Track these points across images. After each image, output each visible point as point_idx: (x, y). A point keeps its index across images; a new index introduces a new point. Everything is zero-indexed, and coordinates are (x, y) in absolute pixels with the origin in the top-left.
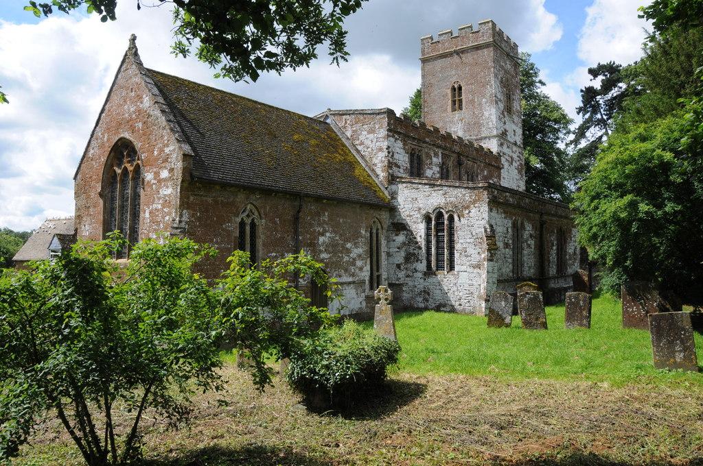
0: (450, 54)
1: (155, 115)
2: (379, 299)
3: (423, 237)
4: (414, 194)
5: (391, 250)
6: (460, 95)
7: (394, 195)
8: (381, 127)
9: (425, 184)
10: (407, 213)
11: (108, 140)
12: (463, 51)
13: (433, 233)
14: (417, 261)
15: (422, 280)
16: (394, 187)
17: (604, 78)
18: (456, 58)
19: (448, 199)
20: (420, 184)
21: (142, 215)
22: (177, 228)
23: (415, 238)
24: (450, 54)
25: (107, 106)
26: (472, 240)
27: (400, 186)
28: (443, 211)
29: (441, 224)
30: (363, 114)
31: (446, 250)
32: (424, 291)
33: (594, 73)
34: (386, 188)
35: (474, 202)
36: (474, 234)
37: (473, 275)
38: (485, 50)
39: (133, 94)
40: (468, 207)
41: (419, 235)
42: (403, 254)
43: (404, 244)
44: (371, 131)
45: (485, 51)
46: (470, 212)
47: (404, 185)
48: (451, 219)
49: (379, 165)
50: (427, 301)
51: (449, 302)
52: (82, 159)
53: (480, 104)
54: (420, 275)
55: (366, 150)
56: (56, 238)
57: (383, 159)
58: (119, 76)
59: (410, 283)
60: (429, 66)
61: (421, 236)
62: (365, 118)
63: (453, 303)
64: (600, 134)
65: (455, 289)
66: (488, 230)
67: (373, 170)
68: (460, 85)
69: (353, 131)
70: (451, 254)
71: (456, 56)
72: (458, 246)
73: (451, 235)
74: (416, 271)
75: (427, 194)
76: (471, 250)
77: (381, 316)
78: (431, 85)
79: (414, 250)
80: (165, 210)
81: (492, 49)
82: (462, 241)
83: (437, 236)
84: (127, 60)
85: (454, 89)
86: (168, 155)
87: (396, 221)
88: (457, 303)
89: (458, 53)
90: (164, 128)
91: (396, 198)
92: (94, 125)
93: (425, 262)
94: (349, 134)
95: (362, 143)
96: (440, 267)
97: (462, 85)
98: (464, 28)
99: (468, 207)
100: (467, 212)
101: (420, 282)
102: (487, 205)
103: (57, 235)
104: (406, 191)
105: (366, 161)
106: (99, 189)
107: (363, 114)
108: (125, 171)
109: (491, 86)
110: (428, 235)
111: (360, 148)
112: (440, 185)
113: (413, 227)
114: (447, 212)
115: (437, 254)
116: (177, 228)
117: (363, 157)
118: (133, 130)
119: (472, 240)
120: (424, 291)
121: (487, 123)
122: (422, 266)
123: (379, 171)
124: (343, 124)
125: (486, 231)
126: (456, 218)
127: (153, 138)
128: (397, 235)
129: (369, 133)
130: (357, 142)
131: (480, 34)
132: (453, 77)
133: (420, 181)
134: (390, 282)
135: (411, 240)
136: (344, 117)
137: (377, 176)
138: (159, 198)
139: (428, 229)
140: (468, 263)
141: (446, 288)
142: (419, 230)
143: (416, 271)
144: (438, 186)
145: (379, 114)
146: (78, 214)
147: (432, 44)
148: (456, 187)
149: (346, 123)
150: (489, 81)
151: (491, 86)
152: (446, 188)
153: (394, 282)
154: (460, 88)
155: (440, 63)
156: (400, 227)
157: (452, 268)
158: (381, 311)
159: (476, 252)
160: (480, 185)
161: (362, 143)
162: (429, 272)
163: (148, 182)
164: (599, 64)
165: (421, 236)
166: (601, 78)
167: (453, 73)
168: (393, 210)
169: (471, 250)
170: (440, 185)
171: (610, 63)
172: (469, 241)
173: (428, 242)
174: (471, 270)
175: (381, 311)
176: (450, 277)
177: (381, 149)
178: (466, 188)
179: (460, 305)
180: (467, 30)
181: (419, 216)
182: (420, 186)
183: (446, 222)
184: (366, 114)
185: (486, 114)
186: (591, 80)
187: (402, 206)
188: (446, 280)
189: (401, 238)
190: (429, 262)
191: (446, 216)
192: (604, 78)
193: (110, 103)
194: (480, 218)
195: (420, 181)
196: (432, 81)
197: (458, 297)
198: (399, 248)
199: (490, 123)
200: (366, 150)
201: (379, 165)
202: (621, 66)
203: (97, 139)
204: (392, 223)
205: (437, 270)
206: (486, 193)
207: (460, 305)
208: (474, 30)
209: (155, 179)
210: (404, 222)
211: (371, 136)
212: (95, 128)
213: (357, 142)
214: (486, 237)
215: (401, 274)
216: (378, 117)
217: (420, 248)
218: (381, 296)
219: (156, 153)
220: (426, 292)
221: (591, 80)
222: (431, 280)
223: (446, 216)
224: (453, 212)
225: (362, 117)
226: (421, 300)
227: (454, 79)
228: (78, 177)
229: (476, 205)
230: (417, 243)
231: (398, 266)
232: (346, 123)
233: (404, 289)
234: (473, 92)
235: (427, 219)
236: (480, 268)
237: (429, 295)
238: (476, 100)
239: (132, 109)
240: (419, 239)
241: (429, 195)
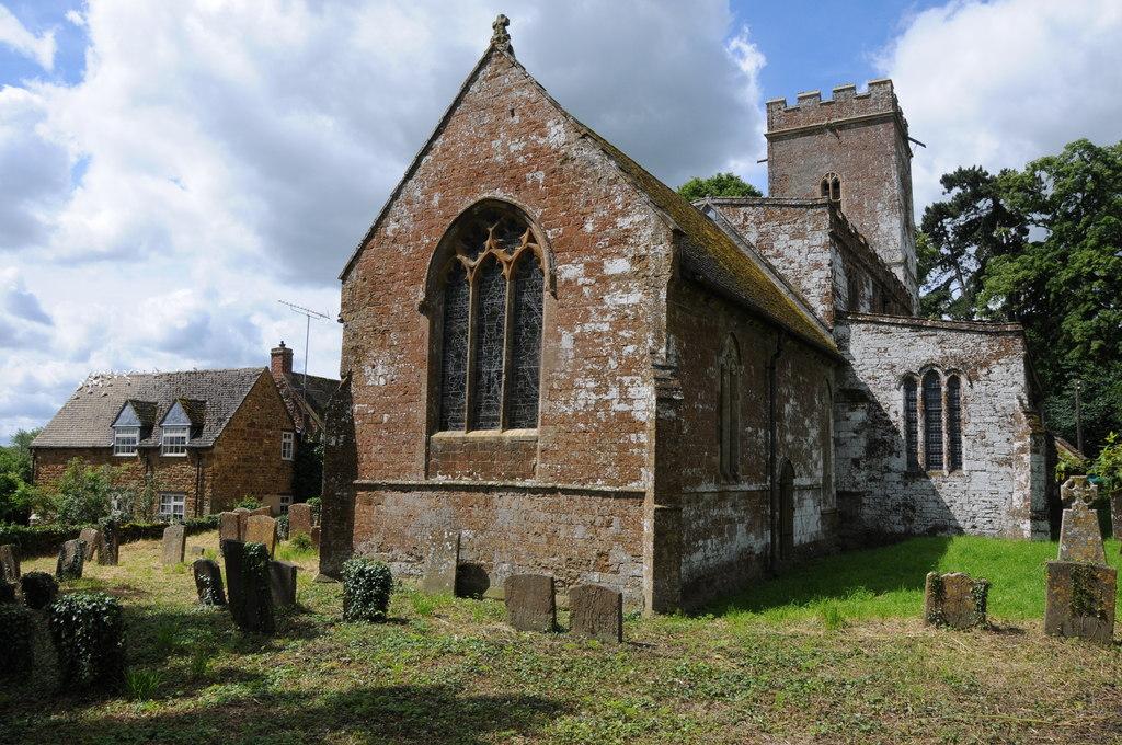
0: (820, 130)
1: (584, 159)
2: (1071, 499)
3: (901, 412)
4: (881, 341)
5: (842, 435)
6: (837, 194)
7: (843, 341)
8: (818, 228)
9: (903, 325)
10: (869, 373)
11: (443, 204)
12: (842, 126)
13: (919, 405)
14: (891, 454)
15: (901, 486)
16: (841, 330)
17: (961, 191)
18: (829, 137)
19: (948, 351)
20: (893, 324)
21: (546, 345)
22: (663, 368)
23: (886, 415)
24: (820, 130)
25: (439, 143)
26: (995, 419)
27: (854, 328)
28: (939, 370)
29: (935, 393)
30: (781, 206)
31: (945, 436)
32: (905, 505)
33: (949, 182)
34: (830, 331)
35: (998, 356)
36: (998, 408)
37: (998, 477)
38: (880, 126)
39: (517, 119)
40: (986, 364)
41: (893, 409)
42: (863, 441)
43: (864, 424)
44: (799, 235)
45: (881, 128)
46: (990, 372)
47: (863, 326)
48: (954, 383)
49: (815, 292)
50: (911, 521)
51: (952, 523)
52: (370, 236)
53: (873, 211)
54: (896, 477)
55: (787, 265)
56: (129, 408)
57: (823, 282)
58: (474, 88)
59: (878, 492)
60: (781, 147)
61: (896, 412)
62: (785, 213)
63: (961, 524)
64: (944, 279)
65: (964, 499)
66: (1026, 402)
67: (804, 302)
68: (836, 180)
69: (762, 234)
70: (955, 442)
71: (829, 133)
72: (968, 429)
73: (954, 410)
74: (889, 470)
75: (907, 341)
76: (993, 435)
77: (1076, 530)
78: (785, 177)
79: (883, 434)
80: (621, 333)
81: (892, 124)
82: (977, 421)
83: (926, 412)
84: (494, 60)
85: (825, 186)
86: (626, 230)
87: (847, 386)
88: (968, 524)
89: (832, 128)
90: (613, 182)
91: (846, 348)
92: (402, 176)
93: (904, 455)
94: (752, 237)
95: (779, 255)
96: (933, 462)
97: (840, 179)
98: (843, 90)
99: (986, 364)
100: (985, 371)
101: (898, 492)
102: (1022, 360)
103: (134, 402)
104: (866, 337)
105: (787, 285)
106: (421, 296)
107: (781, 206)
108: (491, 264)
109: (891, 183)
110: (909, 410)
111: (774, 262)
112: (930, 328)
113: (881, 397)
114: (946, 373)
115: (927, 442)
116: (663, 368)
117: (781, 278)
118: (517, 183)
119: (995, 419)
120: (905, 505)
121: (886, 242)
122: (899, 463)
123: (814, 301)
124: (740, 221)
125: (1022, 403)
126: (964, 382)
127: (579, 201)
128: (852, 410)
129: (793, 237)
130: (769, 253)
131: (872, 100)
132: (826, 167)
133: (893, 320)
134: (840, 489)
135: (878, 416)
136: (742, 209)
137: (811, 310)
138: (604, 313)
139: (910, 400)
140: (988, 457)
141: (946, 499)
142: (894, 402)
143: (889, 470)
144: (926, 328)
145: (812, 206)
146: (354, 344)
147: (785, 111)
148: (964, 331)
149: (746, 219)
150: (888, 176)
151: (891, 183)
152: (943, 333)
153: (847, 489)
154: (836, 185)
155: (799, 144)
156: (859, 396)
157: (955, 464)
158: (1076, 521)
159: (1004, 438)
160: (1009, 328)
161: (779, 255)
162: (914, 473)
163: (568, 282)
164: (960, 169)
165: (896, 412)
166: (957, 190)
167: (825, 159)
168: (841, 364)
169: (993, 435)
170: (930, 328)
171: (974, 168)
172: (989, 419)
173: (910, 422)
174: (996, 467)
175: (1076, 521)
176: (955, 480)
177: (818, 266)
178: (981, 333)
179: (974, 527)
180: (848, 93)
181: (891, 378)
182: (893, 328)
183: (944, 389)
184: (787, 206)
185: (884, 227)
186: (944, 193)
187: (858, 362)
188: (948, 486)
189: (859, 415)
190: (912, 453)
191: (944, 379)
192: (961, 191)
193: (447, 136)
194: (1010, 383)
195: (893, 320)
196: (787, 171)
197: (971, 514)
198: (855, 432)
199: (891, 243)
200: (787, 265)
201: (815, 292)
202: (987, 174)
203: (409, 203)
204: (841, 390)
205: (928, 468)
206: (1019, 341)
207: (974, 527)
208: (790, 107)
209: (587, 275)
210: (864, 388)
211: (798, 243)
212: (405, 181)
213: (769, 253)
214: (1025, 412)
215: (861, 476)
216: (811, 212)
217: (896, 432)
218: (1076, 494)
219: (589, 227)
220: (909, 507)
221: (944, 193)
222: (919, 485)
223: (944, 379)
224: (959, 372)
225: (778, 211)
226: (898, 519)
227: (827, 170)
228: (354, 274)
229: (1002, 361)
230: (889, 423)
231: (856, 462)
232: (746, 219)
233: (865, 501)
234: (860, 192)
235: (908, 382)
236: (1011, 465)
237: (913, 509)
238: (866, 205)
239: (513, 148)
240: (892, 417)
241: (911, 344)
